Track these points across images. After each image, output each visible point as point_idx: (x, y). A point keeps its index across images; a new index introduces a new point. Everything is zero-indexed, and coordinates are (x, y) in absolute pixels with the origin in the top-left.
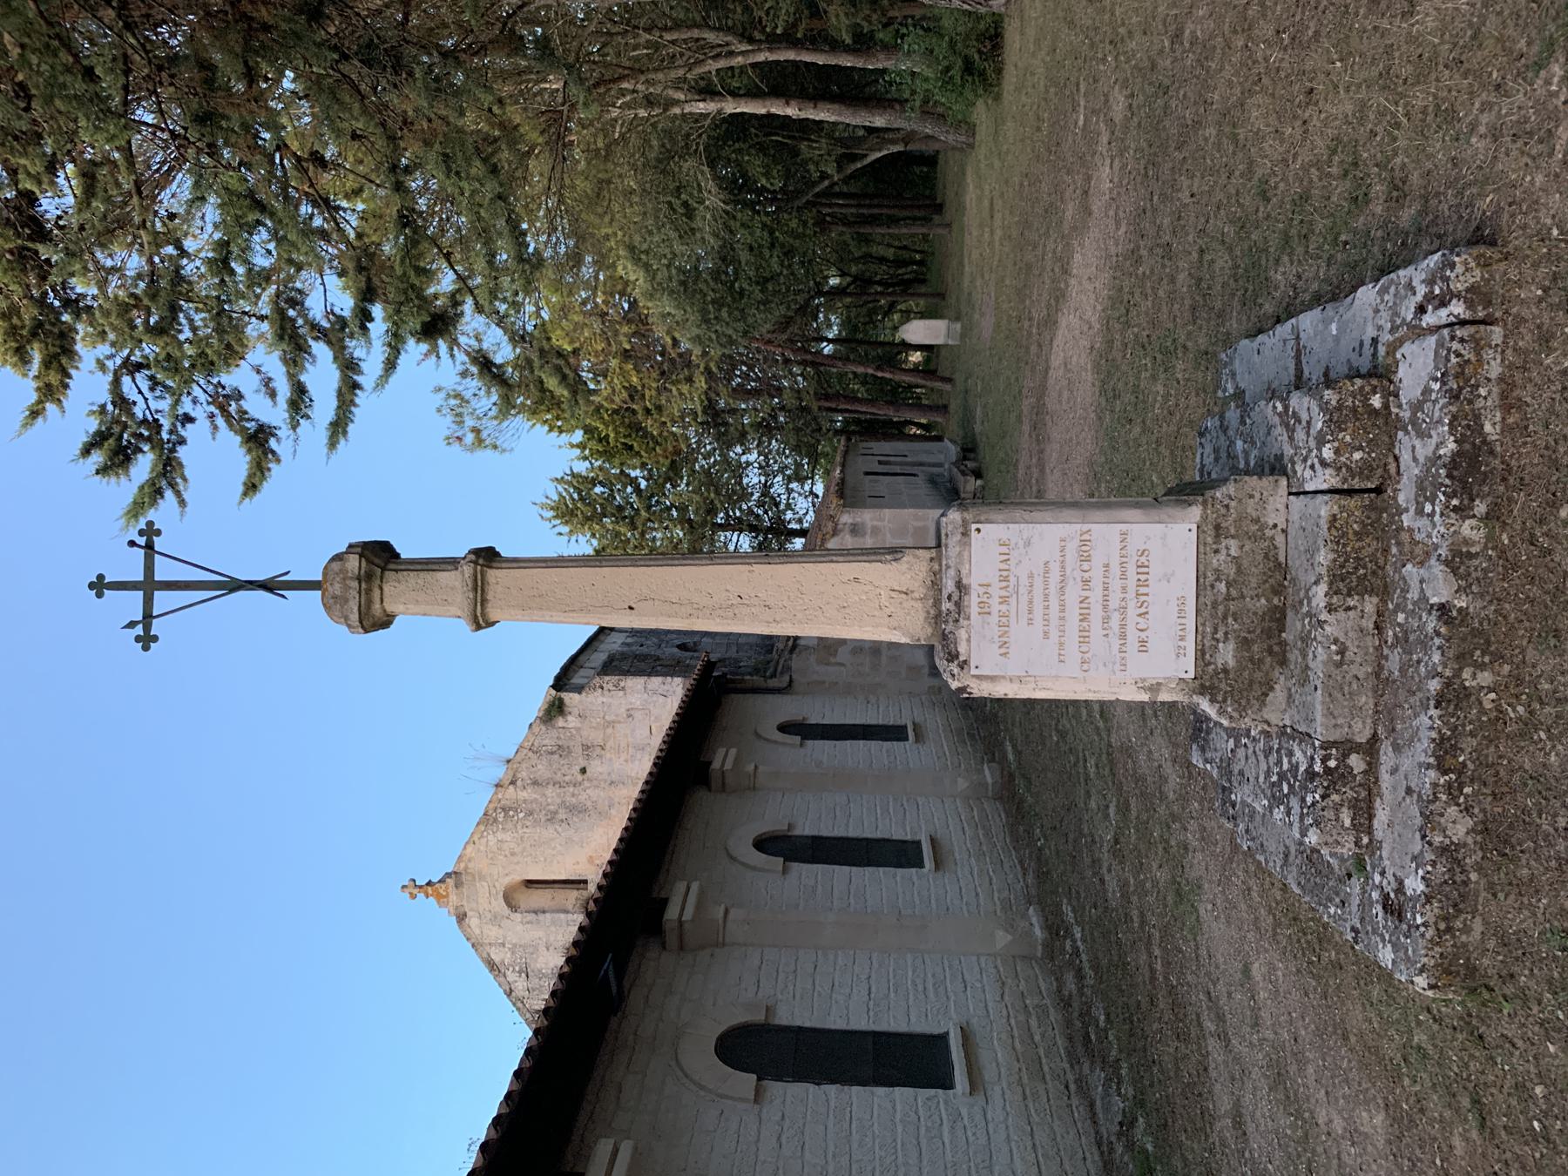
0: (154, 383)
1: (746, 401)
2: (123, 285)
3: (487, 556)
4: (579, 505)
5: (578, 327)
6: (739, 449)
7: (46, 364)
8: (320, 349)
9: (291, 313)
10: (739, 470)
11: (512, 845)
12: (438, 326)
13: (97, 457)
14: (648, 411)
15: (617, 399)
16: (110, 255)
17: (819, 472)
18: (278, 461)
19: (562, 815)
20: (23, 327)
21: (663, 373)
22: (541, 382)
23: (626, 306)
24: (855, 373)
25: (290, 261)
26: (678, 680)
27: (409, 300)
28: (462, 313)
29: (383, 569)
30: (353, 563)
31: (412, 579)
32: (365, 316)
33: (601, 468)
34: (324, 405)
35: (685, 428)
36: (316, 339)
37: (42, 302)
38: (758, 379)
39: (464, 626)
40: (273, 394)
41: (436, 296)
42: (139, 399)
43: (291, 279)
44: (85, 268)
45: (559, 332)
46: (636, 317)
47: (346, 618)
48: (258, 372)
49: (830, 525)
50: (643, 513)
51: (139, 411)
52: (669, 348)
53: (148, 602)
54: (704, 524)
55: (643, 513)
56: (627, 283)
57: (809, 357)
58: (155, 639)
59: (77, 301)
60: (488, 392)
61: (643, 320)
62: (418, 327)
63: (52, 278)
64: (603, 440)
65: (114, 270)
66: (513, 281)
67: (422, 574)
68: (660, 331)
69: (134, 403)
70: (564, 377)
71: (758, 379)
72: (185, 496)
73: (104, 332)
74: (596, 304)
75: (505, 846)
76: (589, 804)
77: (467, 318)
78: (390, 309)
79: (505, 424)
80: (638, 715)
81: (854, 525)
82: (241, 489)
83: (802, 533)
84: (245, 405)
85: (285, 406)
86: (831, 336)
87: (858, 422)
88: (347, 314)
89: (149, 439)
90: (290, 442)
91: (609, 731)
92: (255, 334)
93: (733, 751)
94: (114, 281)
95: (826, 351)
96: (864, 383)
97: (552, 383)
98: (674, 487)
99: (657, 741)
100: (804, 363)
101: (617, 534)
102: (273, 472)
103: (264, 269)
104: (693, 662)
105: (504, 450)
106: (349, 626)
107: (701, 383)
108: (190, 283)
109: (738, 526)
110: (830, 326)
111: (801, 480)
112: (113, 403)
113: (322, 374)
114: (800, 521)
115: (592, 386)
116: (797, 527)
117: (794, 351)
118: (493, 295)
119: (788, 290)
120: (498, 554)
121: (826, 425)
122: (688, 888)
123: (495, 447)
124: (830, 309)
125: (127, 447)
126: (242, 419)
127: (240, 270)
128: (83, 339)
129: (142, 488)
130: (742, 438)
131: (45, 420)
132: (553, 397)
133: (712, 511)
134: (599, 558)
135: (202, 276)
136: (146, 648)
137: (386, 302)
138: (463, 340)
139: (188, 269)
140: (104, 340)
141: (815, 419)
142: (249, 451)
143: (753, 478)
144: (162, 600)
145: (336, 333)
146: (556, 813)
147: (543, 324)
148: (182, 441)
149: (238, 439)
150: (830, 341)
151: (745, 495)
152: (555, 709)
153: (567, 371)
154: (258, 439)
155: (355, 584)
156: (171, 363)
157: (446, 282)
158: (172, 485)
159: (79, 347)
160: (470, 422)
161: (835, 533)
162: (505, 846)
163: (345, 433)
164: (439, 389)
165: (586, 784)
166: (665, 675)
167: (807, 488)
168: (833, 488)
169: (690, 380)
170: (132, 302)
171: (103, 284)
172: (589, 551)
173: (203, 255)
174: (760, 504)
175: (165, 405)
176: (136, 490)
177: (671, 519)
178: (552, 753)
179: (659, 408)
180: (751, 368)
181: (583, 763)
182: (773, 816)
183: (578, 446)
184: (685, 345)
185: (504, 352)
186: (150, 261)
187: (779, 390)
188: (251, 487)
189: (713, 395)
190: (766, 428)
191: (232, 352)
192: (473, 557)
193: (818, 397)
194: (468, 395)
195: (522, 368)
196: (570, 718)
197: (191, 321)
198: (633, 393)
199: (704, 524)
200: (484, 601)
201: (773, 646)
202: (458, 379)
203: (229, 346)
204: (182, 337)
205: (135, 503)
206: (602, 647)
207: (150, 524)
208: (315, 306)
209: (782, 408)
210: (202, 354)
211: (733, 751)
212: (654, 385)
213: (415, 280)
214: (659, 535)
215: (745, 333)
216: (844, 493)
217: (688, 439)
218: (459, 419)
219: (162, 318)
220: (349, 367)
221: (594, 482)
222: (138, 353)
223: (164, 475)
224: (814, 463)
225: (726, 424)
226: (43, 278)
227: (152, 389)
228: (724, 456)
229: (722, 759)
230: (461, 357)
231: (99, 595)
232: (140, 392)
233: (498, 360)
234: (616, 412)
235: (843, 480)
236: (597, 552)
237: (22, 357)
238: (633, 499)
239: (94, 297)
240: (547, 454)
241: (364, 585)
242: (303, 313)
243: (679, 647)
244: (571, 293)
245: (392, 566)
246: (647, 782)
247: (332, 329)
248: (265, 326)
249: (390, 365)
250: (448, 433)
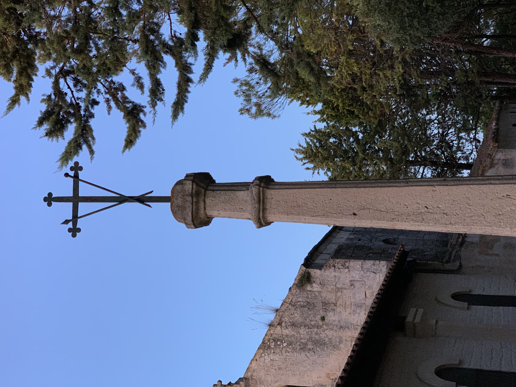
0: (77, 82)
1: (429, 79)
2: (60, 26)
3: (266, 182)
4: (317, 150)
5: (321, 37)
6: (424, 112)
7: (20, 73)
8: (169, 59)
9: (152, 37)
10: (425, 124)
11: (280, 363)
12: (236, 42)
13: (46, 126)
14: (364, 89)
15: (344, 82)
16: (53, 9)
17: (481, 125)
18: (144, 126)
19: (310, 346)
20: (9, 53)
21: (374, 64)
22: (297, 73)
23: (351, 22)
24: (506, 59)
25: (151, 6)
26: (383, 263)
27: (220, 26)
28: (250, 33)
29: (206, 190)
30: (189, 186)
31: (223, 196)
32: (193, 37)
33: (333, 126)
34: (171, 93)
35: (388, 99)
36: (166, 53)
37: (17, 38)
38: (438, 65)
39: (251, 224)
40: (141, 86)
41: (235, 23)
42: (68, 91)
43: (152, 17)
44: (41, 17)
45: (308, 41)
46: (358, 30)
47: (185, 219)
48: (133, 74)
49: (488, 160)
50: (360, 155)
51: (68, 99)
52: (378, 48)
53: (75, 209)
54: (400, 161)
55: (360, 155)
56: (351, 7)
57: (473, 49)
58: (79, 230)
59: (36, 36)
60: (266, 82)
61: (362, 31)
62: (225, 43)
63: (23, 24)
64: (335, 108)
65: (55, 17)
66: (282, 10)
67: (228, 192)
68: (372, 37)
69: (66, 94)
70: (312, 70)
71: (438, 65)
72: (94, 148)
73: (50, 54)
74: (332, 22)
75: (275, 363)
76: (327, 339)
77: (253, 36)
78: (210, 32)
79: (276, 100)
80: (357, 285)
81: (506, 160)
82: (123, 143)
83: (468, 166)
84: (126, 93)
85: (149, 94)
86: (489, 34)
87: (508, 90)
88: (183, 36)
89: (73, 115)
90: (151, 115)
91: (339, 294)
92: (131, 51)
93: (421, 311)
94: (55, 24)
95: (485, 44)
96: (511, 64)
97: (304, 74)
98: (380, 137)
99: (370, 301)
100: (470, 52)
101: (344, 168)
102: (142, 133)
103: (136, 11)
104: (394, 252)
105: (274, 117)
106: (186, 223)
107: (399, 69)
108: (96, 22)
109: (424, 162)
110: (488, 27)
111: (468, 131)
112: (55, 94)
113: (169, 75)
114: (467, 158)
115: (329, 75)
116: (465, 162)
117: (464, 45)
118: (270, 20)
119: (459, 5)
120: (272, 180)
121: (485, 93)
122: (417, 311)
123: (269, 115)
124: (488, 15)
125: (62, 120)
126: (125, 102)
127: (124, 13)
128: (39, 58)
129: (70, 143)
130: (427, 104)
131: (19, 105)
132: (304, 82)
133: (406, 153)
134: (332, 183)
135: (102, 18)
136: (74, 236)
137: (206, 28)
138: (251, 49)
139: (95, 13)
140: (50, 58)
141: (478, 89)
142: (128, 121)
143: (434, 130)
144: (83, 208)
145: (179, 48)
146: (306, 344)
147: (299, 37)
148: (92, 116)
149: (122, 114)
150: (488, 37)
151: (428, 141)
152: (304, 280)
153: (314, 66)
154: (133, 114)
155: (190, 199)
156: (86, 70)
157: (241, 13)
158: (87, 142)
159: (36, 63)
160: (254, 100)
161: (492, 165)
162: (275, 363)
163: (182, 109)
164: (236, 81)
165: (325, 327)
166: (375, 259)
167: (472, 136)
168: (490, 136)
169: (392, 67)
170: (65, 35)
171: (49, 26)
172: (326, 179)
173: (102, 5)
174: (439, 147)
175: (83, 94)
176: (66, 144)
177: (379, 159)
178: (304, 307)
179: (371, 87)
180: (433, 58)
181: (322, 314)
182: (449, 354)
183: (318, 113)
184: (389, 45)
185: (275, 56)
186: (75, 11)
187: (453, 71)
188: (130, 142)
189: (407, 77)
190: (444, 97)
191: (119, 63)
192: (258, 182)
193: (479, 74)
194: (253, 83)
195: (286, 65)
196: (314, 285)
197: (96, 45)
198: (354, 78)
199: (400, 161)
200: (264, 209)
201: (447, 242)
202: (247, 74)
203: (118, 59)
204: (91, 55)
205: (66, 152)
206: (334, 240)
207: (77, 163)
208: (165, 32)
209: (455, 83)
210: (104, 64)
211: (421, 311)
212: (368, 72)
213: (223, 14)
214: (370, 169)
215: (429, 35)
216: (499, 139)
217: (390, 106)
218: (248, 100)
219: (81, 44)
220: (185, 69)
221: (329, 135)
222: (68, 65)
223: (82, 136)
224: (477, 120)
225: (416, 95)
226: (19, 24)
227: (75, 86)
228: (414, 116)
229: (414, 315)
230: (250, 60)
231: (50, 205)
232: (69, 88)
233: (272, 61)
234: (343, 90)
235: (497, 129)
236: (331, 179)
237: (8, 71)
238: (355, 145)
239: (45, 34)
240: (299, 119)
241: (194, 200)
242: (159, 36)
243: (384, 241)
244: (316, 16)
245: (210, 188)
246: (363, 328)
247: (175, 46)
248: (137, 46)
249: (209, 67)
250: (241, 107)
